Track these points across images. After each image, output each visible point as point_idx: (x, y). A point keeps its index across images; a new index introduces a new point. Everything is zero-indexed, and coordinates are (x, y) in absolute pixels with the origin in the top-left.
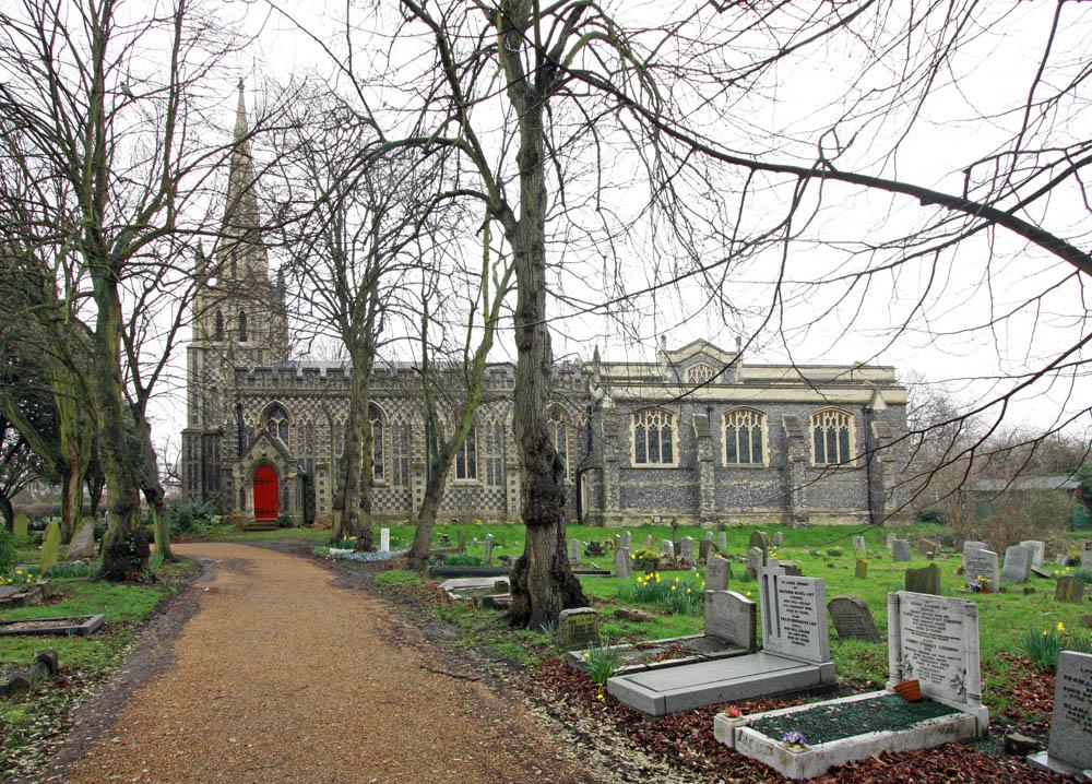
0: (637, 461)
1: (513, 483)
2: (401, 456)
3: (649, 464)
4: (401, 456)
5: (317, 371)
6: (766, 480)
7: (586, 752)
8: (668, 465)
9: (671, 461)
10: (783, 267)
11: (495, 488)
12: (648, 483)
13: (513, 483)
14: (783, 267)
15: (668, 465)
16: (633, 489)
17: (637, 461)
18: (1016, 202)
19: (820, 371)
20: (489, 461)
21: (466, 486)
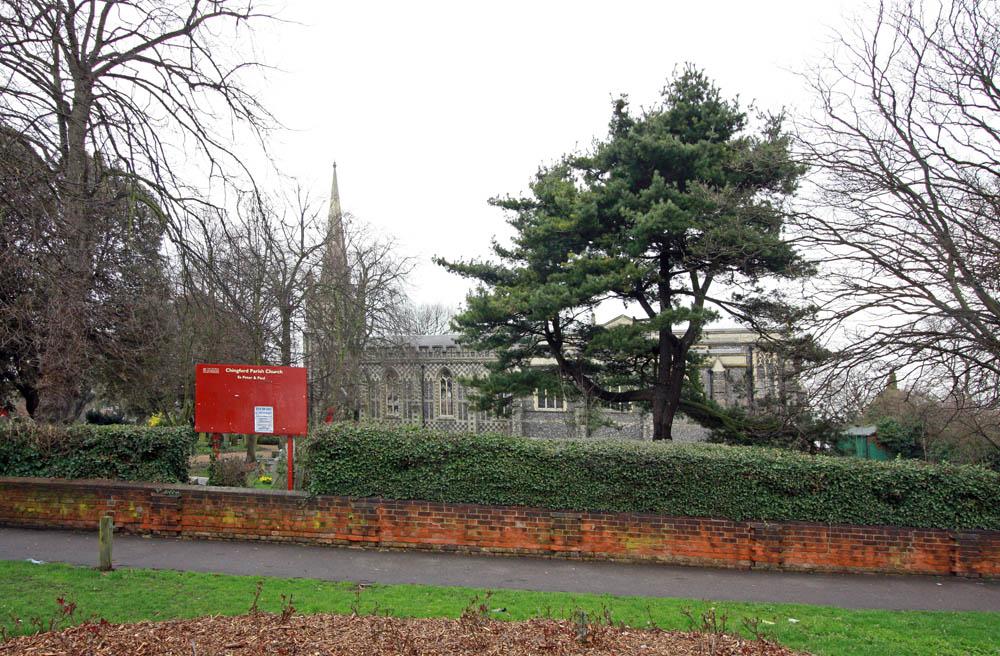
0: (540, 406)
1: (472, 418)
2: (408, 400)
3: (546, 409)
4: (408, 400)
5: (441, 347)
6: (630, 421)
7: (21, 327)
8: (560, 410)
9: (562, 407)
10: (842, 121)
11: (463, 422)
12: (545, 421)
13: (472, 418)
14: (842, 121)
15: (560, 410)
16: (535, 425)
17: (540, 406)
18: (181, 110)
19: (720, 336)
20: (460, 404)
21: (446, 420)
